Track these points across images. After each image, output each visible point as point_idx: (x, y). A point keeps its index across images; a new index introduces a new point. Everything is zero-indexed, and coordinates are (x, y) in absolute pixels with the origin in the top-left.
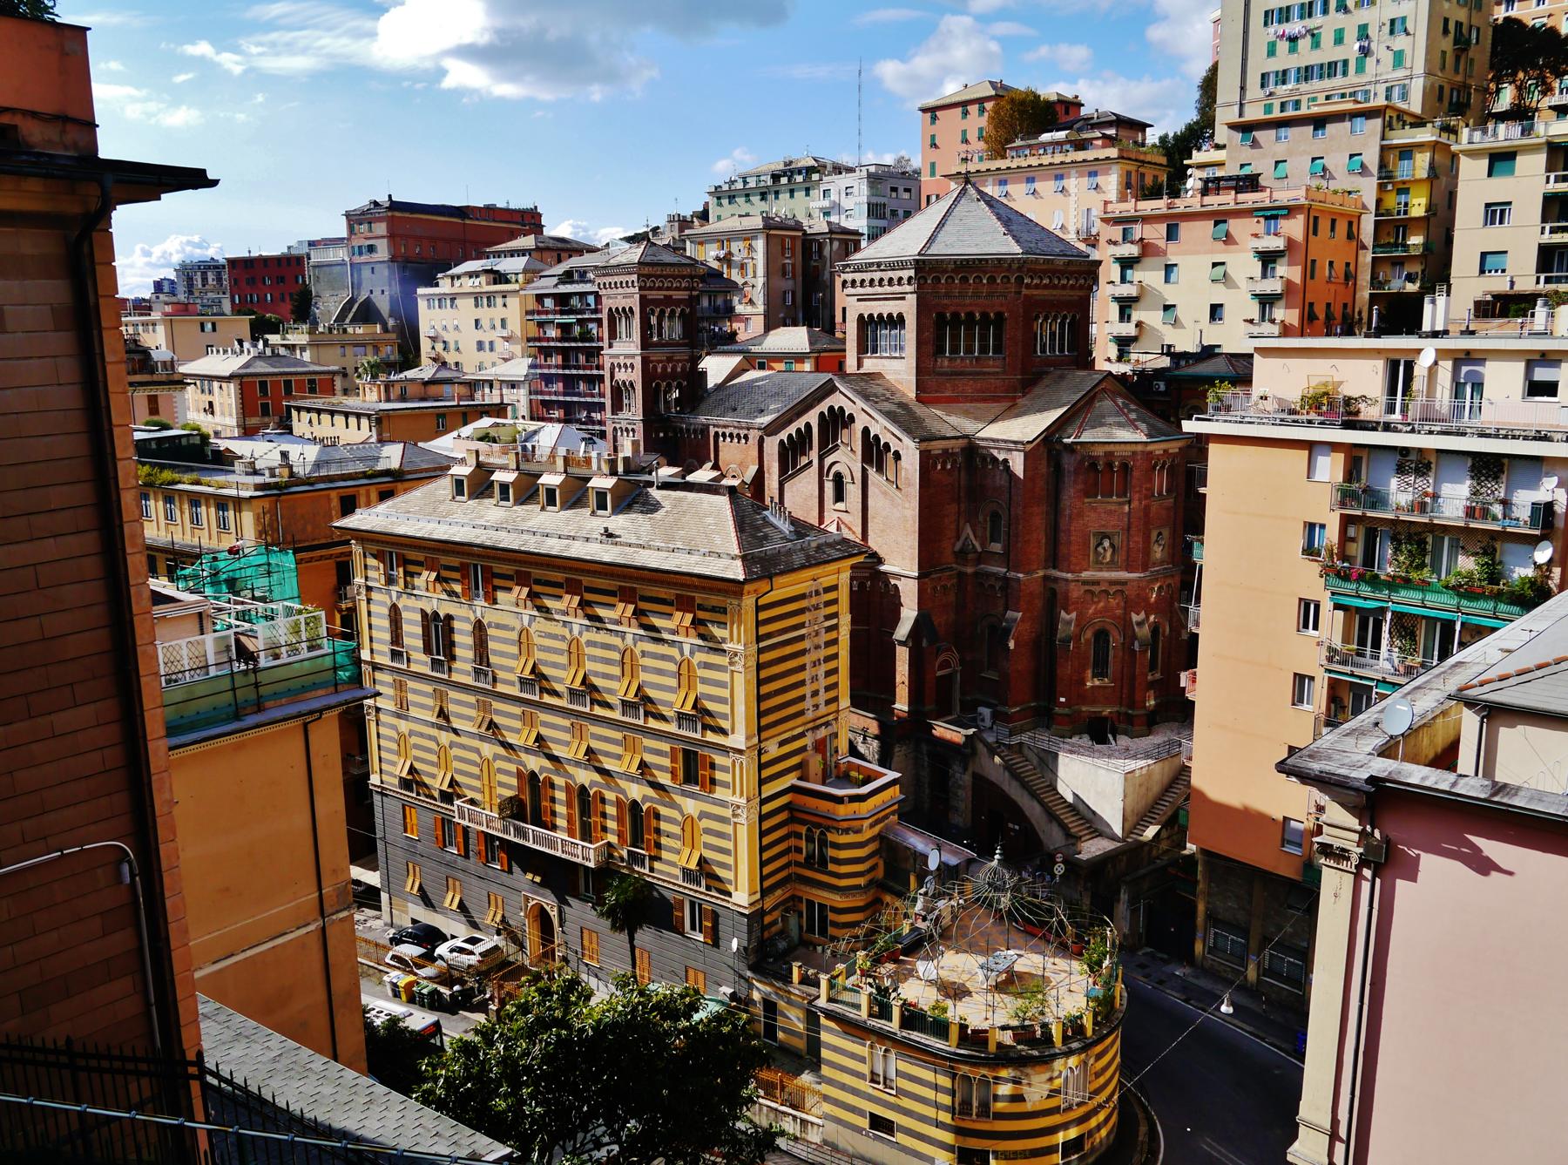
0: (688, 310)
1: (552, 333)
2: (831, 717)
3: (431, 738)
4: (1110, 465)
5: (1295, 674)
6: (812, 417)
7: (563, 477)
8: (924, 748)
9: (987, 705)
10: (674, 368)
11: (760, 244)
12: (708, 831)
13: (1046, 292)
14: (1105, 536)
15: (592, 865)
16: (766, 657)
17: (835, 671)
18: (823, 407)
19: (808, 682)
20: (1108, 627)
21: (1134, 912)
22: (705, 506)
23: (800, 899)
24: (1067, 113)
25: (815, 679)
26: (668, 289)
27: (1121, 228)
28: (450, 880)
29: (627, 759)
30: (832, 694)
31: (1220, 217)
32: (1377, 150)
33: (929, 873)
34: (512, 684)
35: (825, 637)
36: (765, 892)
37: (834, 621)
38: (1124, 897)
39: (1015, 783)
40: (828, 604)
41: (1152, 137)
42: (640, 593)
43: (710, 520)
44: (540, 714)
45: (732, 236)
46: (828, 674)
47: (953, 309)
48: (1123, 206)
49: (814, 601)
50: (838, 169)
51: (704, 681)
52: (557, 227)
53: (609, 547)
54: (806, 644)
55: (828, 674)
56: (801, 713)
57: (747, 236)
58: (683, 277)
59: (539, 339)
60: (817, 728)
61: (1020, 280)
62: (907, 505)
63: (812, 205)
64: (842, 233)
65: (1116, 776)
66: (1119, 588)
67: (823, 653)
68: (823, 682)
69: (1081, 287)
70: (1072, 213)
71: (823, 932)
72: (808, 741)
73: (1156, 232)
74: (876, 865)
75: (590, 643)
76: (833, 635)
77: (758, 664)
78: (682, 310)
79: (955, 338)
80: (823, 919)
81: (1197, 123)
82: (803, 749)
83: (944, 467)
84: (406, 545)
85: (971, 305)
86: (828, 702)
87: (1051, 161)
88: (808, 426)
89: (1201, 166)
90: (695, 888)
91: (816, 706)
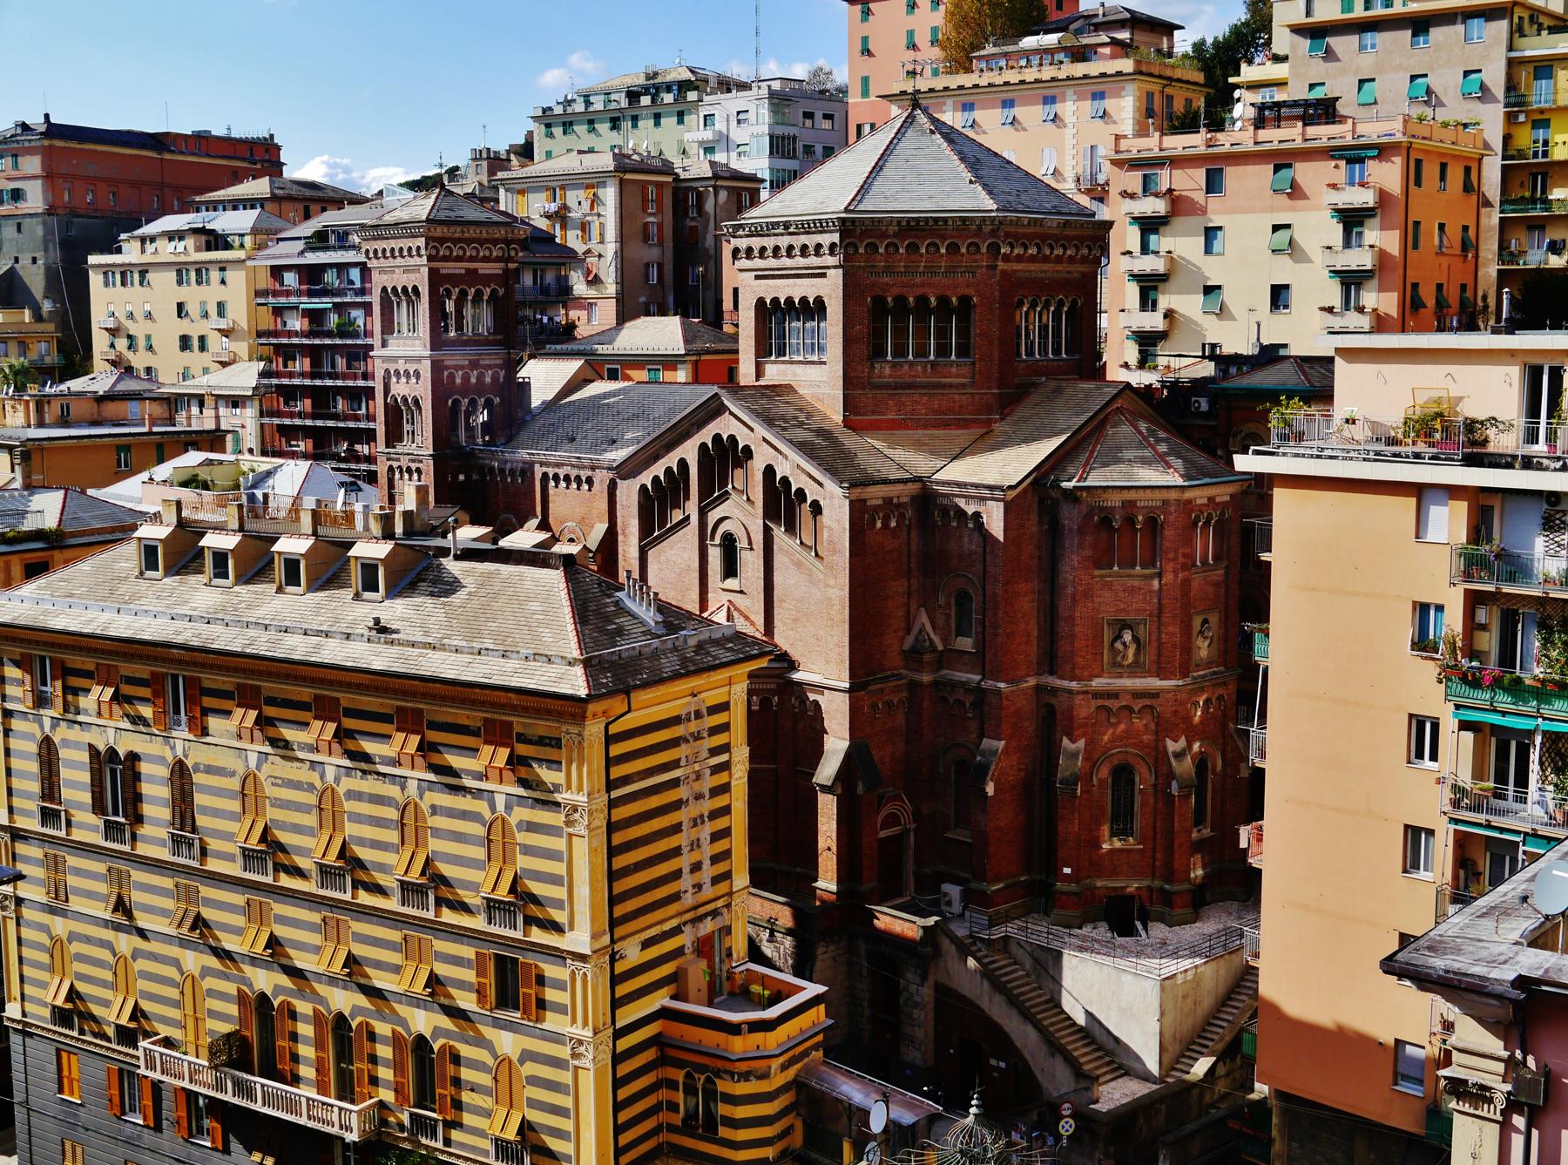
0: (501, 292)
1: (296, 323)
2: (720, 903)
3: (107, 945)
4: (1130, 521)
6: (689, 451)
7: (237, 538)
9: (955, 881)
10: (480, 378)
11: (610, 194)
12: (534, 1081)
13: (1032, 267)
14: (1126, 625)
16: (621, 813)
17: (725, 833)
18: (706, 435)
19: (685, 850)
20: (1133, 761)
25: (695, 845)
26: (472, 259)
27: (1139, 174)
30: (721, 868)
31: (1282, 160)
34: (230, 858)
35: (710, 782)
37: (724, 758)
40: (714, 731)
41: (1183, 43)
43: (535, 606)
44: (201, 888)
46: (716, 837)
47: (896, 291)
48: (1143, 143)
49: (693, 726)
51: (528, 850)
53: (381, 648)
54: (682, 792)
55: (716, 837)
56: (676, 897)
57: (591, 181)
58: (495, 242)
59: (269, 334)
61: (993, 249)
66: (1147, 702)
67: (707, 805)
68: (708, 850)
72: (686, 939)
75: (353, 795)
78: (494, 292)
79: (901, 333)
81: (1246, 24)
82: (679, 952)
83: (886, 525)
85: (922, 285)
86: (716, 880)
87: (1038, 76)
88: (683, 464)
89: (1254, 86)
91: (698, 887)
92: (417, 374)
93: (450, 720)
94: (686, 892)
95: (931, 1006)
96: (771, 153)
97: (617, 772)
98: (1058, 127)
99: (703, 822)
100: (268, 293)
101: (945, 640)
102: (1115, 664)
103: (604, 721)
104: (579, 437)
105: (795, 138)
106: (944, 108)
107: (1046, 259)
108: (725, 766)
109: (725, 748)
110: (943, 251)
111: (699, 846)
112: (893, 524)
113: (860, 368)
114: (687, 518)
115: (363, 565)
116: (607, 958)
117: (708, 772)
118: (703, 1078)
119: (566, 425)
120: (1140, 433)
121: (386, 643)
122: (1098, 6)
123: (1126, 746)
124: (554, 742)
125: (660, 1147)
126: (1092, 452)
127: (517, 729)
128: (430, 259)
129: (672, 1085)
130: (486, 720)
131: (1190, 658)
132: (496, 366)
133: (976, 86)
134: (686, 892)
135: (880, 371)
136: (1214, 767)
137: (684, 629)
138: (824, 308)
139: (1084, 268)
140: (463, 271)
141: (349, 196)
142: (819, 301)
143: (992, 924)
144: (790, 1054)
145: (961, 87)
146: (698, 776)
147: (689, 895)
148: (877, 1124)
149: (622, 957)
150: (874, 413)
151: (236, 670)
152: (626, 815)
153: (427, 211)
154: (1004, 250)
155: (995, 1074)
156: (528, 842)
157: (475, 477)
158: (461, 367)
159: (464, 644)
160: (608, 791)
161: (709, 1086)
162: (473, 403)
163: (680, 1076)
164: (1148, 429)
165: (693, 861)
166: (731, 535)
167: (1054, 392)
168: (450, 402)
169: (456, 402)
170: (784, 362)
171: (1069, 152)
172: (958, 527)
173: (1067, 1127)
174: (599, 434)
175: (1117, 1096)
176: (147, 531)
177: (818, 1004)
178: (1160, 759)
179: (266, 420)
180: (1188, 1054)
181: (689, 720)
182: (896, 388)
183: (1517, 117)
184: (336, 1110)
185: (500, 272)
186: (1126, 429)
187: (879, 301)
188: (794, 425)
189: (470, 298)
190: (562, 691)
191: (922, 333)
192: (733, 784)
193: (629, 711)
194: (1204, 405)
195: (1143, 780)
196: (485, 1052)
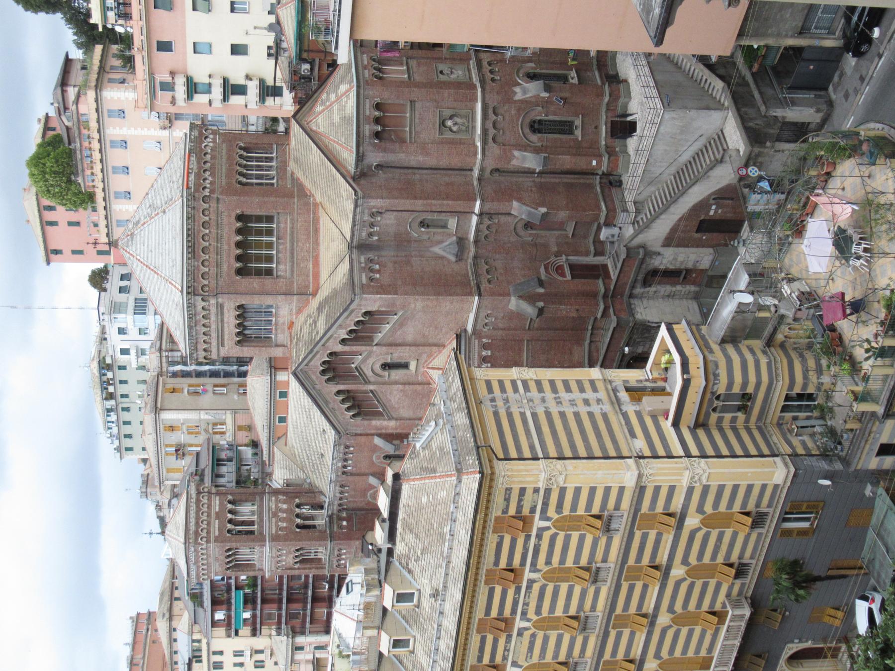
0: (230, 497)
2: (609, 387)
8: (638, 290)
9: (599, 229)
10: (284, 511)
14: (443, 124)
17: (566, 383)
18: (320, 381)
19: (576, 409)
20: (528, 121)
21: (794, 103)
22: (411, 503)
23: (780, 418)
24: (54, 129)
25: (573, 403)
26: (209, 515)
27: (159, 93)
30: (587, 386)
33: (755, 301)
35: (534, 393)
37: (519, 384)
38: (779, 113)
39: (672, 209)
40: (503, 389)
41: (77, 54)
42: (491, 566)
43: (424, 500)
44: (642, 512)
46: (568, 389)
47: (233, 260)
48: (140, 88)
49: (500, 403)
51: (574, 508)
52: (151, 602)
53: (448, 594)
54: (540, 411)
55: (568, 389)
56: (605, 416)
60: (618, 400)
62: (413, 306)
63: (134, 365)
64: (161, 339)
65: (667, 116)
66: (491, 111)
67: (549, 395)
68: (576, 395)
70: (145, 132)
71: (810, 397)
72: (630, 409)
73: (164, 60)
74: (748, 347)
75: (538, 612)
76: (532, 385)
77: (559, 459)
78: (230, 502)
79: (259, 258)
80: (800, 397)
81: (65, 14)
82: (639, 414)
83: (378, 272)
85: (229, 245)
86: (595, 390)
87: (98, 151)
88: (339, 393)
89: (105, 18)
90: (770, 518)
91: (599, 401)
93: (493, 553)
94: (601, 409)
95: (676, 250)
96: (144, 314)
97: (527, 453)
99: (559, 398)
100: (231, 627)
101: (450, 235)
102: (467, 131)
103: (495, 461)
104: (321, 451)
105: (136, 299)
108: (525, 383)
109: (514, 382)
111: (574, 400)
112: (377, 267)
113: (280, 284)
114: (372, 391)
115: (397, 602)
116: (641, 461)
117: (528, 394)
118: (716, 402)
119: (313, 458)
120: (323, 111)
121: (445, 591)
122: (53, 107)
123: (518, 125)
124: (508, 492)
125: (759, 429)
126: (334, 142)
127: (499, 513)
129: (720, 420)
130: (494, 532)
131: (463, 83)
132: (276, 500)
133: (104, 190)
134: (601, 409)
135: (283, 271)
136: (532, 68)
137: (440, 408)
140: (217, 521)
141: (169, 577)
143: (625, 210)
144: (703, 348)
146: (530, 400)
147: (604, 408)
148: (748, 299)
149: (641, 451)
150: (308, 276)
152: (554, 447)
154: (207, 192)
155: (720, 211)
156: (569, 508)
157: (344, 515)
158: (277, 522)
159: (447, 544)
160: (538, 459)
161: (722, 398)
162: (298, 516)
163: (714, 417)
164: (321, 105)
165: (582, 404)
166: (382, 365)
167: (296, 163)
168: (298, 530)
169: (298, 526)
170: (276, 330)
171: (145, 132)
172: (380, 227)
173: (753, 171)
174: (319, 439)
175: (735, 138)
176: (385, 646)
177: (673, 329)
178: (527, 104)
179: (307, 631)
180: (710, 92)
181: (496, 406)
182: (293, 262)
185: (218, 498)
186: (321, 120)
187: (239, 272)
188: (316, 326)
189: (233, 517)
190: (477, 488)
191: (259, 245)
193: (490, 446)
194: (306, 67)
195: (539, 114)
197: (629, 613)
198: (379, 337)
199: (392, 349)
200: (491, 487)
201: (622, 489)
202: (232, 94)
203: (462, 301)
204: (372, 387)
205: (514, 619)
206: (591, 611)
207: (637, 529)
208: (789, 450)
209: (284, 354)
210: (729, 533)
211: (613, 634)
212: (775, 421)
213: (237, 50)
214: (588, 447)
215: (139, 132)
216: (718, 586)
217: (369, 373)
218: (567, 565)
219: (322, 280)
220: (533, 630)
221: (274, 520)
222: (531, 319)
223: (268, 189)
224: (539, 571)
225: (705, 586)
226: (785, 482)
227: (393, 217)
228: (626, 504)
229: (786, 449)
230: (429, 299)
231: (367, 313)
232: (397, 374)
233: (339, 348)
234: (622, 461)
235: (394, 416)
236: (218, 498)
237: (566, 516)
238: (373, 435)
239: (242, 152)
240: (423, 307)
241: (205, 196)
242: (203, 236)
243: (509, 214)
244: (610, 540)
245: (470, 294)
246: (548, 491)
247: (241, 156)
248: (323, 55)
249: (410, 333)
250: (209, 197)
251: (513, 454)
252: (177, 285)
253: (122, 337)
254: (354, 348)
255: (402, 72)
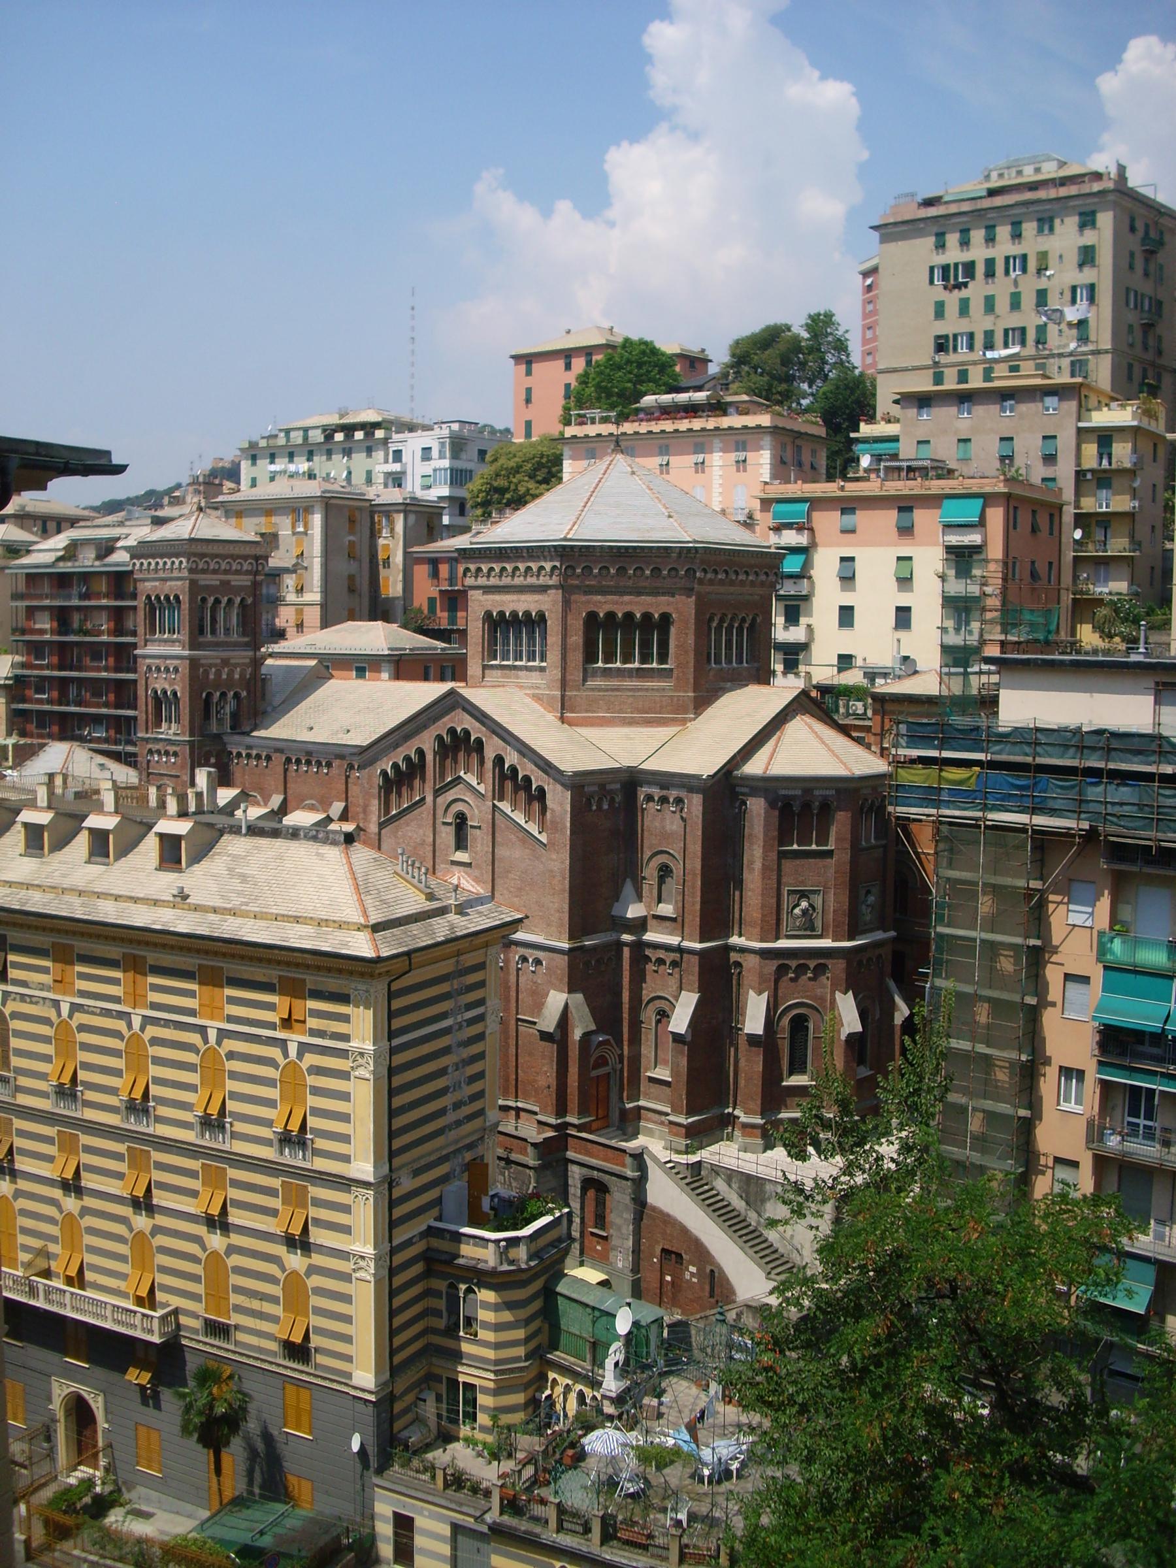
0: (250, 601)
1: (44, 623)
3: (197, 1240)
4: (807, 806)
5: (1061, 1067)
6: (426, 741)
7: (116, 820)
11: (317, 519)
12: (92, 1231)
13: (722, 589)
15: (156, 1339)
16: (399, 1059)
18: (441, 728)
23: (439, 1379)
26: (226, 572)
28: (142, 1431)
29: (205, 1195)
31: (905, 506)
32: (1073, 432)
33: (617, 1337)
34: (43, 1094)
36: (395, 1371)
44: (310, 1188)
45: (270, 508)
50: (411, 428)
51: (317, 1091)
57: (298, 509)
58: (245, 558)
59: (23, 632)
61: (690, 572)
69: (762, 584)
78: (243, 600)
84: (74, 933)
85: (630, 603)
88: (421, 753)
92: (176, 670)
96: (451, 483)
98: (738, 470)
105: (471, 471)
106: (762, 443)
107: (732, 583)
110: (648, 572)
112: (605, 807)
114: (423, 799)
116: (386, 1186)
127: (150, 961)
128: (191, 571)
129: (437, 1294)
132: (244, 664)
138: (545, 621)
139: (759, 591)
142: (542, 617)
145: (599, 435)
149: (398, 1184)
150: (587, 711)
151: (198, 951)
153: (189, 530)
158: (215, 665)
160: (389, 1040)
161: (452, 1291)
162: (223, 695)
168: (204, 695)
169: (209, 695)
182: (607, 690)
183: (1085, 475)
184: (68, 1295)
185: (249, 583)
189: (223, 605)
192: (487, 1033)
196: (54, 1209)
197: (81, 1154)
198: (505, 806)
199: (487, 827)
200: (351, 973)
201: (346, 1159)
202: (786, 606)
203: (562, 925)
204: (429, 799)
205: (73, 994)
206: (232, 1132)
207: (283, 1182)
208: (398, 1390)
209: (472, 676)
210: (277, 1310)
211: (121, 1148)
212: (437, 1371)
213: (846, 615)
214: (403, 1109)
215: (717, 481)
216: (195, 1297)
217: (451, 795)
218: (12, 1039)
219: (579, 729)
220: (203, 1048)
221: (219, 661)
222: (535, 1023)
223: (703, 657)
224: (142, 1029)
225: (195, 1278)
226: (355, 1388)
227: (674, 827)
228: (321, 1164)
229: (399, 1388)
230: (564, 878)
231: (541, 791)
232: (447, 835)
233: (490, 754)
234: (386, 1159)
235: (383, 831)
236: (249, 583)
237: (224, 1065)
238: (347, 800)
239: (749, 622)
240: (552, 871)
241: (695, 572)
242: (640, 568)
243: (681, 989)
244: (267, 1142)
245: (572, 937)
246: (343, 1054)
247: (743, 620)
248: (878, 731)
249: (512, 853)
250: (695, 577)
251: (397, 1004)
252: (572, 532)
253: (419, 454)
254: (489, 775)
255: (868, 840)
